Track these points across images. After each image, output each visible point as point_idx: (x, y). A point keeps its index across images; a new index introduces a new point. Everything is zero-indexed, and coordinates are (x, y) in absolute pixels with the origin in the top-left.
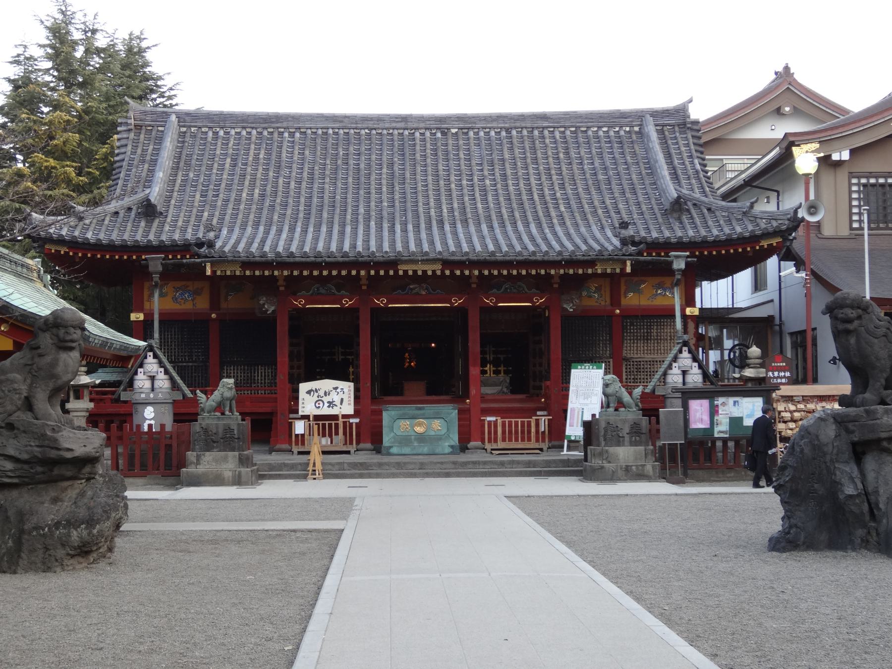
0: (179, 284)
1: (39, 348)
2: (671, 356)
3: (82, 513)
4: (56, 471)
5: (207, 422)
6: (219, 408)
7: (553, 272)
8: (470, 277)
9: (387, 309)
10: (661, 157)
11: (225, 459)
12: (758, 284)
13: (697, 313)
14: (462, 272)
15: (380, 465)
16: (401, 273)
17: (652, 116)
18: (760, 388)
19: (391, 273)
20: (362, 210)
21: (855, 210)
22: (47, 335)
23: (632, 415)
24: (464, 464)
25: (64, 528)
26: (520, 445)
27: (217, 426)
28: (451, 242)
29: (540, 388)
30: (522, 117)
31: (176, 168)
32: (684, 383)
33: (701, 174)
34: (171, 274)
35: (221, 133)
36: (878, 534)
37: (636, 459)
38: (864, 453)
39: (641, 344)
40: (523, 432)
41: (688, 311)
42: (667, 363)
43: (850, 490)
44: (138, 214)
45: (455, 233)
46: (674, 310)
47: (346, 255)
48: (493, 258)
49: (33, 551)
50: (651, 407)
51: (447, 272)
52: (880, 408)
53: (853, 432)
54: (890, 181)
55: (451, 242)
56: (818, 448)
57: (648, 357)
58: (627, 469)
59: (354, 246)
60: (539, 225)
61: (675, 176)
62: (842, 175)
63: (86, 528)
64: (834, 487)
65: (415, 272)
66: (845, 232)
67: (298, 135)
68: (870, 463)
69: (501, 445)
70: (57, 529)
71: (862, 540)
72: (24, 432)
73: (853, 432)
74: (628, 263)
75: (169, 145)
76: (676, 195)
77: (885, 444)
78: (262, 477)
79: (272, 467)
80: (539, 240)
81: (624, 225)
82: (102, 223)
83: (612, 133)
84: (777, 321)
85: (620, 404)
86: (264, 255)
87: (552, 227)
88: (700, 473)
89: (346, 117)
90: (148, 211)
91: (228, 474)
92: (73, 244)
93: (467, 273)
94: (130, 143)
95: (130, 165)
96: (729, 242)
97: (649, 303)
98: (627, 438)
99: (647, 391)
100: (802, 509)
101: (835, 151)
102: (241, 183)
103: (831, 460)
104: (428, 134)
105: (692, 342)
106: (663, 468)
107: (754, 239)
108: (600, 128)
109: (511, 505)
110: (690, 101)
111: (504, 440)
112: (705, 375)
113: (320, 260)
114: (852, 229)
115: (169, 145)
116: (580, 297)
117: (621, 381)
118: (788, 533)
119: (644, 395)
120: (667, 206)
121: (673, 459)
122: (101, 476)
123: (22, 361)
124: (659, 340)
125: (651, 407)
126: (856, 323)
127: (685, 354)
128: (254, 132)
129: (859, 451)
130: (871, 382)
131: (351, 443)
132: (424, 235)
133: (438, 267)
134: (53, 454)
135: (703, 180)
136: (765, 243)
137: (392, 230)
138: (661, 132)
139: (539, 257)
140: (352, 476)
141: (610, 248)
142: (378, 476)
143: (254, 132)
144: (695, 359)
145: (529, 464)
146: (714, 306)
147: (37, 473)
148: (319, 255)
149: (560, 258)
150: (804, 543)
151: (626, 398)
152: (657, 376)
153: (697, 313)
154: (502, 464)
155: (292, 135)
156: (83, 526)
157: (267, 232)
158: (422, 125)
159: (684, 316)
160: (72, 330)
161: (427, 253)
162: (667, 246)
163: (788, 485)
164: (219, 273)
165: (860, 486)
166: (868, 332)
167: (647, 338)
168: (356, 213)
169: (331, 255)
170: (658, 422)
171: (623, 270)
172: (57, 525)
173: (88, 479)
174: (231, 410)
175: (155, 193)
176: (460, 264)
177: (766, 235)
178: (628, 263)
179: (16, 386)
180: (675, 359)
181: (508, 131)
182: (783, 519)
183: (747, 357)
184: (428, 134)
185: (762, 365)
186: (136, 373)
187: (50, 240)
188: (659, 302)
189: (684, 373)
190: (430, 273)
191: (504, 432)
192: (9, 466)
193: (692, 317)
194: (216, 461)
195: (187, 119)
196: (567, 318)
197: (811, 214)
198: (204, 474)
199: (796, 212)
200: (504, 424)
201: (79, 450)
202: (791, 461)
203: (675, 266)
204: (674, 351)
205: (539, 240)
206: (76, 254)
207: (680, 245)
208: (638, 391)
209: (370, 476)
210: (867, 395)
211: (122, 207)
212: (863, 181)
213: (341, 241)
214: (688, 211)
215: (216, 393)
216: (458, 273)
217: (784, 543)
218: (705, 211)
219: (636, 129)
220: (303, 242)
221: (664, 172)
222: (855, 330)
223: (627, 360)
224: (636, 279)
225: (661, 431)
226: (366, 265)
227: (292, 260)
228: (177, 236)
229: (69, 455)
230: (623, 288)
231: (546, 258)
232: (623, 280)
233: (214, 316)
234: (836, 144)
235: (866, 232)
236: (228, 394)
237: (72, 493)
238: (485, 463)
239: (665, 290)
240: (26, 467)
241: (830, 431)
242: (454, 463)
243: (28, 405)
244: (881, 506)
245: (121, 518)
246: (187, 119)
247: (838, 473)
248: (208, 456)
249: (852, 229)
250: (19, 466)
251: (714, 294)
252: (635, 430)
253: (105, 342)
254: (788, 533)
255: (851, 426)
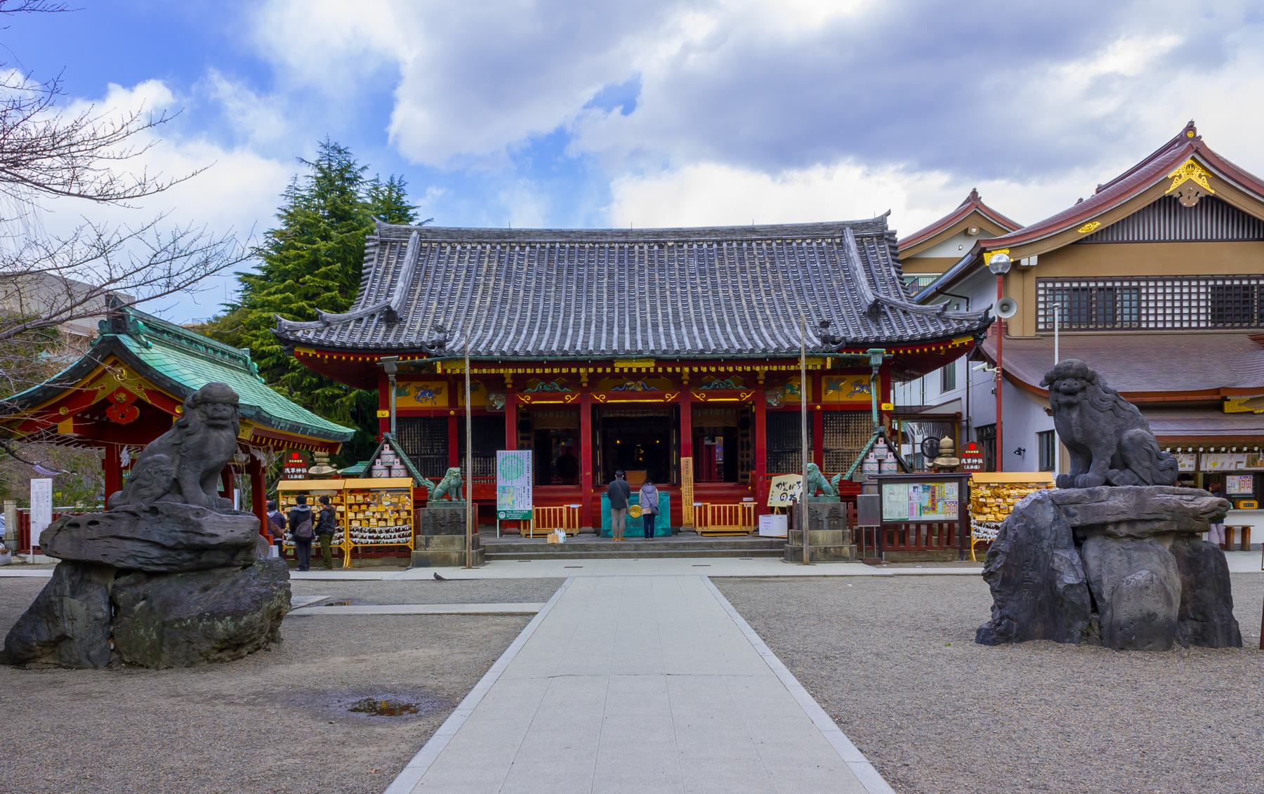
0: (420, 384)
1: (186, 426)
2: (868, 446)
3: (229, 605)
4: (205, 558)
5: (435, 507)
6: (446, 494)
7: (758, 369)
8: (681, 374)
9: (607, 406)
10: (859, 265)
11: (452, 542)
12: (947, 384)
13: (892, 408)
14: (674, 369)
15: (598, 547)
16: (617, 370)
17: (852, 228)
18: (959, 476)
19: (608, 370)
20: (583, 315)
21: (1041, 313)
22: (197, 412)
23: (831, 500)
24: (676, 546)
25: (208, 620)
26: (728, 528)
27: (444, 511)
28: (663, 342)
29: (747, 477)
30: (733, 231)
31: (414, 282)
32: (880, 471)
33: (897, 281)
34: (409, 376)
35: (459, 247)
36: (1100, 627)
37: (834, 542)
38: (1085, 539)
39: (840, 437)
40: (731, 516)
41: (884, 407)
42: (864, 452)
43: (1070, 579)
44: (380, 320)
45: (668, 335)
46: (870, 405)
47: (565, 353)
48: (702, 356)
49: (174, 645)
50: (849, 491)
51: (660, 370)
52: (1106, 489)
53: (1074, 515)
54: (1261, 282)
55: (663, 342)
56: (1035, 533)
57: (847, 449)
58: (826, 550)
59: (573, 346)
60: (746, 328)
61: (872, 283)
62: (1030, 281)
63: (232, 620)
64: (1052, 576)
65: (630, 369)
66: (1032, 333)
67: (528, 249)
68: (1093, 548)
69: (711, 528)
70: (200, 620)
71: (1082, 633)
72: (168, 516)
73: (1074, 515)
74: (829, 360)
75: (409, 257)
76: (872, 299)
77: (1111, 528)
78: (490, 558)
79: (499, 549)
80: (746, 340)
81: (825, 324)
82: (351, 329)
83: (814, 245)
84: (965, 418)
85: (819, 490)
86: (490, 353)
87: (757, 329)
88: (894, 555)
89: (572, 232)
90: (390, 317)
91: (455, 556)
92: (320, 347)
93: (678, 370)
94: (375, 257)
95: (375, 276)
96: (924, 341)
97: (848, 399)
98: (826, 522)
99: (845, 478)
100: (1015, 598)
101: (1024, 256)
102: (474, 291)
103: (1049, 546)
104: (646, 247)
105: (888, 435)
106: (860, 549)
107: (947, 338)
108: (804, 240)
109: (712, 586)
110: (889, 213)
111: (713, 523)
112: (899, 462)
113: (541, 358)
114: (1037, 330)
115: (409, 257)
116: (784, 394)
117: (821, 470)
118: (999, 625)
119: (841, 482)
120: (865, 309)
121: (869, 541)
122: (260, 562)
123: (170, 441)
124: (856, 432)
125: (849, 491)
126: (1080, 395)
127: (881, 444)
128: (488, 246)
129: (1079, 537)
130: (1095, 460)
131: (574, 526)
132: (639, 337)
133: (651, 364)
134: (198, 540)
135: (899, 286)
136: (957, 342)
137: (610, 332)
138: (860, 243)
139: (745, 355)
140: (572, 557)
141: (812, 346)
142: (596, 557)
143: (488, 246)
144: (890, 449)
145: (736, 545)
146: (908, 404)
147: (184, 561)
148: (541, 353)
149: (764, 355)
150: (1017, 635)
151: (825, 484)
152: (855, 465)
153: (892, 408)
154: (710, 545)
155: (523, 249)
156: (228, 618)
157: (495, 335)
158: (641, 239)
159: (880, 412)
160: (221, 407)
161: (640, 352)
162: (865, 345)
163: (1000, 573)
164: (449, 371)
165: (1082, 574)
166: (1092, 404)
167: (845, 432)
168: (577, 318)
169: (552, 353)
170: (855, 507)
171: (824, 366)
172: (201, 617)
173: (245, 567)
174: (458, 497)
175: (395, 301)
176: (672, 362)
177: (959, 334)
178: (829, 360)
179: (162, 467)
180: (872, 448)
181: (719, 243)
182: (993, 609)
183: (938, 447)
184: (646, 247)
185: (954, 455)
186: (374, 463)
187: (298, 342)
188: (857, 398)
189: (880, 462)
190: (644, 370)
191: (713, 516)
192: (155, 552)
193: (888, 413)
194: (444, 543)
195: (429, 235)
196: (772, 414)
197: (1004, 311)
198: (433, 556)
199: (987, 313)
200: (713, 509)
201: (225, 535)
202: (1004, 546)
203: (873, 362)
204: (871, 442)
205: (746, 340)
206: (323, 356)
207: (878, 344)
208: (836, 478)
209: (588, 557)
210: (1090, 475)
211: (366, 314)
212: (1050, 285)
213: (562, 342)
214: (885, 313)
215: (443, 481)
216: (670, 370)
217: (996, 634)
218: (901, 314)
219: (838, 240)
220: (526, 343)
221: (862, 278)
222: (1078, 404)
223: (827, 451)
224: (835, 377)
225: (50, 503)
226: (584, 363)
227: (515, 358)
228: (413, 340)
229: (213, 541)
230: (824, 386)
231: (751, 355)
232: (824, 378)
233: (452, 413)
234: (1026, 251)
235: (1056, 333)
236: (453, 482)
237: (225, 583)
238: (695, 545)
239: (862, 387)
240: (173, 554)
241: (1048, 515)
242: (666, 545)
243: (176, 486)
244: (1105, 596)
245: (280, 607)
246: (429, 235)
247: (1056, 560)
248: (436, 539)
249: (1037, 330)
250: (165, 552)
251: (906, 394)
252: (834, 514)
253: (295, 427)
254: (999, 625)
255: (1071, 509)
